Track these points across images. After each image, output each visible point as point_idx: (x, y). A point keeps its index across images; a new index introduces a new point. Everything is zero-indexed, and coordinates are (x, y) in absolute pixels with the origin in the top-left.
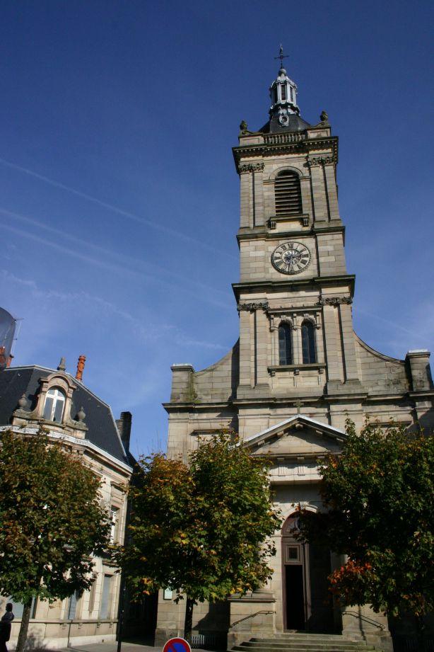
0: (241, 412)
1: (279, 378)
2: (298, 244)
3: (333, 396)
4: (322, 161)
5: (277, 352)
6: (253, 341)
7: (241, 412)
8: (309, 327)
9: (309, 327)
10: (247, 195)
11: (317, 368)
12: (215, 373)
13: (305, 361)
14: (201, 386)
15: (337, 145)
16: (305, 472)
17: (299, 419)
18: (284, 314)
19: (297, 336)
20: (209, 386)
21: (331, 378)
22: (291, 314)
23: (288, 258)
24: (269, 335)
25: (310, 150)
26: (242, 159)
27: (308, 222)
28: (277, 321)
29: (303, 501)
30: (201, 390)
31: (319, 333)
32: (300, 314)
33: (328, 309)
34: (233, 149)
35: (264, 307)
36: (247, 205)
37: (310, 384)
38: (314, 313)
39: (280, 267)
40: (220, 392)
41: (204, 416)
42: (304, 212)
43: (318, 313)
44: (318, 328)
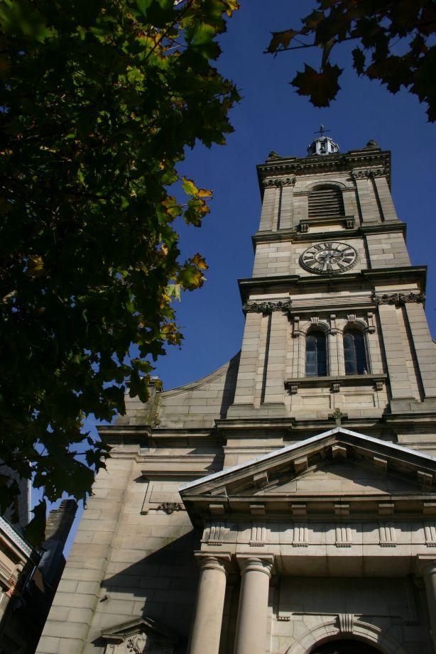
0: (230, 443)
1: (303, 397)
2: (338, 245)
3: (404, 416)
4: (371, 173)
5: (303, 362)
6: (263, 350)
7: (230, 443)
8: (356, 336)
9: (356, 336)
10: (270, 204)
11: (372, 382)
12: (195, 393)
13: (349, 369)
14: (168, 410)
15: (390, 162)
16: (351, 540)
17: (339, 436)
18: (315, 315)
19: (336, 344)
20: (183, 410)
21: (395, 395)
22: (327, 315)
23: (323, 259)
24: (291, 341)
25: (355, 167)
26: (251, 297)
27: (353, 224)
28: (304, 325)
29: (346, 612)
30: (168, 416)
31: (372, 339)
32: (341, 314)
33: (384, 309)
34: (257, 166)
35: (286, 309)
36: (251, 384)
37: (363, 404)
38: (363, 313)
39: (313, 267)
40: (200, 418)
41: (166, 452)
42: (346, 215)
43: (370, 314)
44: (371, 332)
